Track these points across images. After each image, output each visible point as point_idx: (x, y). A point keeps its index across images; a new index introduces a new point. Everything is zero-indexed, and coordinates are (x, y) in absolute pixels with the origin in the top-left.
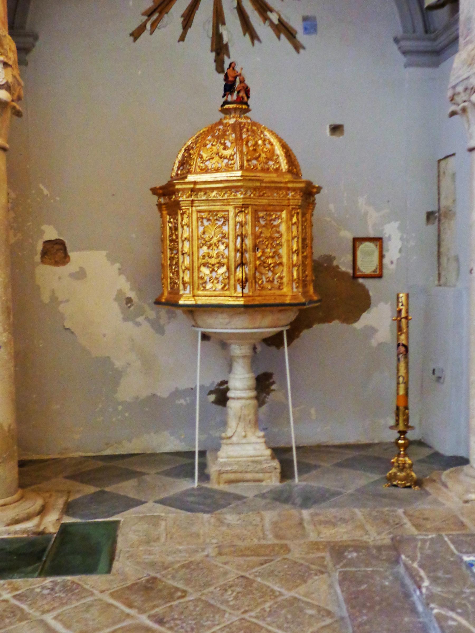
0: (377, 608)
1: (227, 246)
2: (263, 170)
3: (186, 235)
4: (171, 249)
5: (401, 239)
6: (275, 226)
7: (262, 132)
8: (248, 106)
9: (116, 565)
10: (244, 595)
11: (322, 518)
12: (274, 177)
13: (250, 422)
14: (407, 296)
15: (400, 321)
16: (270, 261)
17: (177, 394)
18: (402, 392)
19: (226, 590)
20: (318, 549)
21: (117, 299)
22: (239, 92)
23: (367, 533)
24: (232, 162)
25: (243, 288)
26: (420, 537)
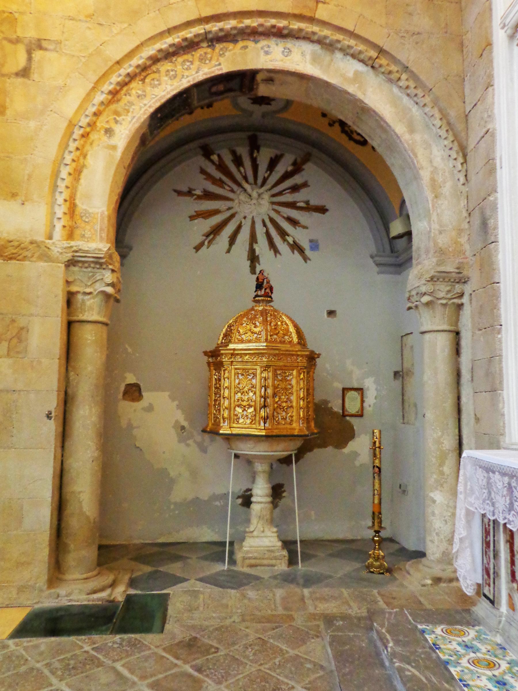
0: (357, 662)
1: (255, 393)
2: (281, 342)
3: (226, 385)
4: (215, 394)
5: (376, 389)
6: (288, 380)
7: (281, 316)
8: (272, 298)
9: (167, 627)
10: (260, 652)
11: (318, 595)
12: (288, 347)
13: (267, 520)
14: (380, 431)
15: (375, 449)
16: (284, 404)
17: (215, 497)
18: (376, 501)
19: (247, 648)
20: (315, 619)
21: (174, 427)
22: (265, 289)
23: (350, 607)
24: (260, 336)
25: (265, 423)
26: (388, 610)
